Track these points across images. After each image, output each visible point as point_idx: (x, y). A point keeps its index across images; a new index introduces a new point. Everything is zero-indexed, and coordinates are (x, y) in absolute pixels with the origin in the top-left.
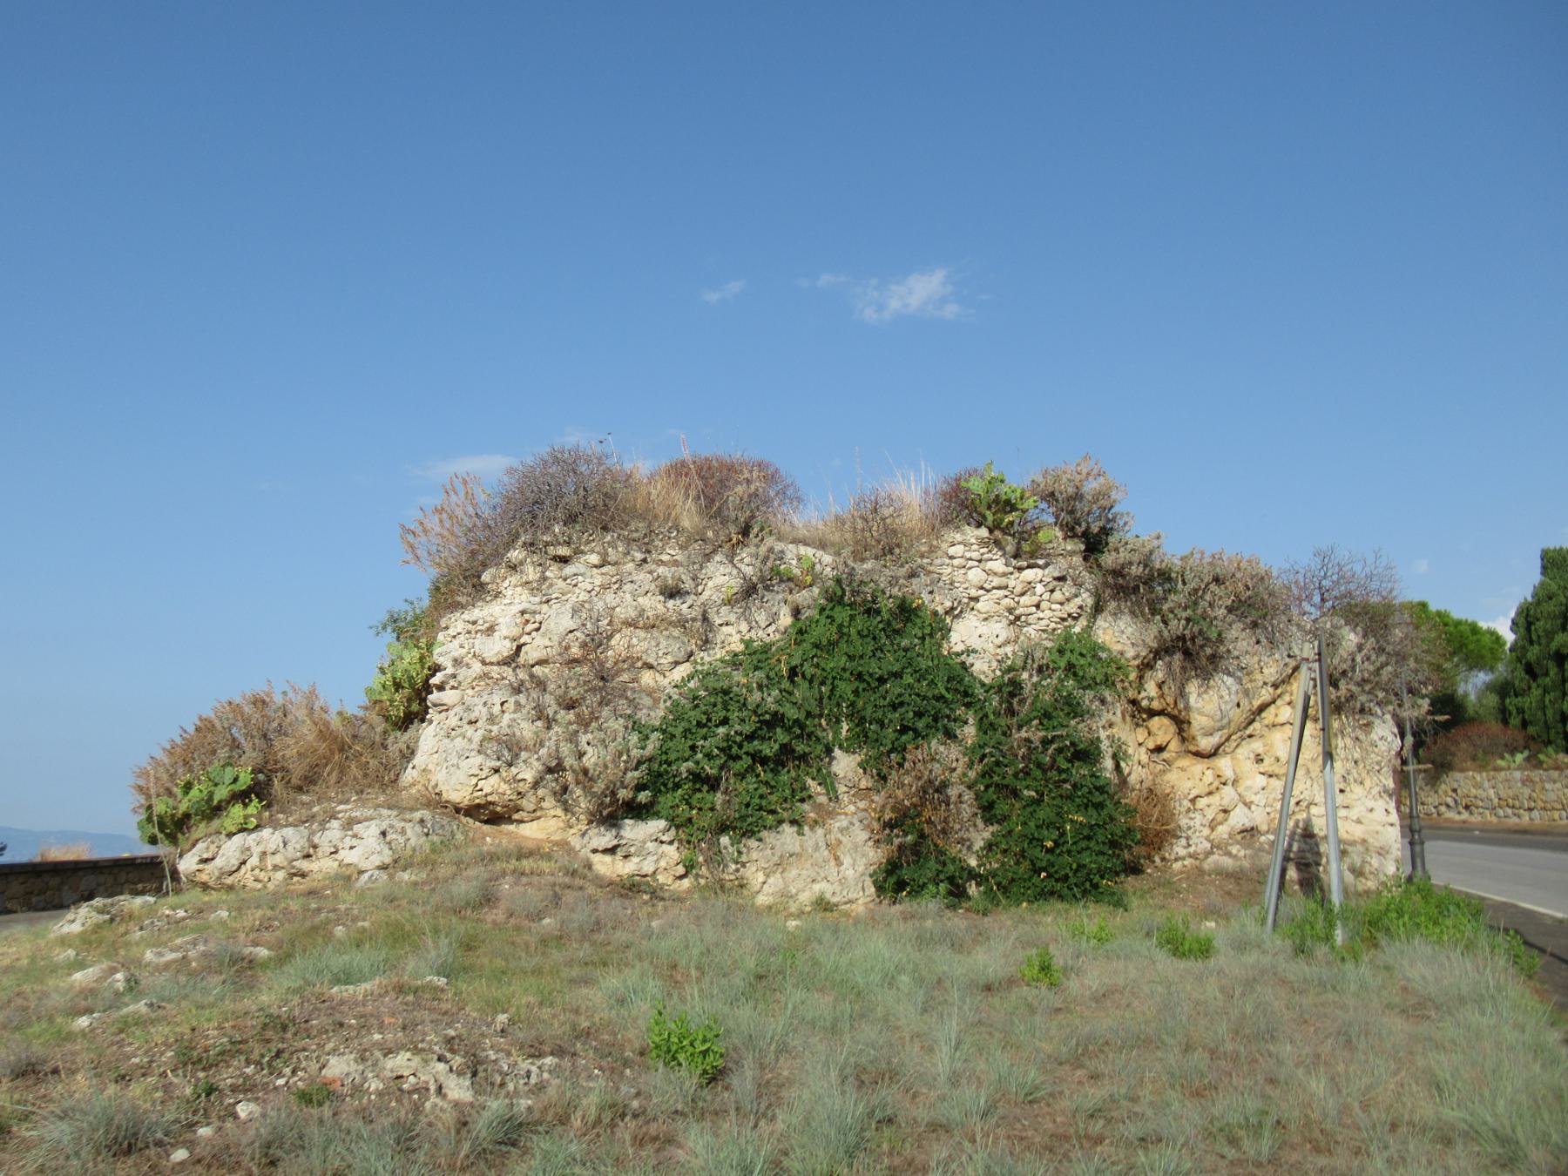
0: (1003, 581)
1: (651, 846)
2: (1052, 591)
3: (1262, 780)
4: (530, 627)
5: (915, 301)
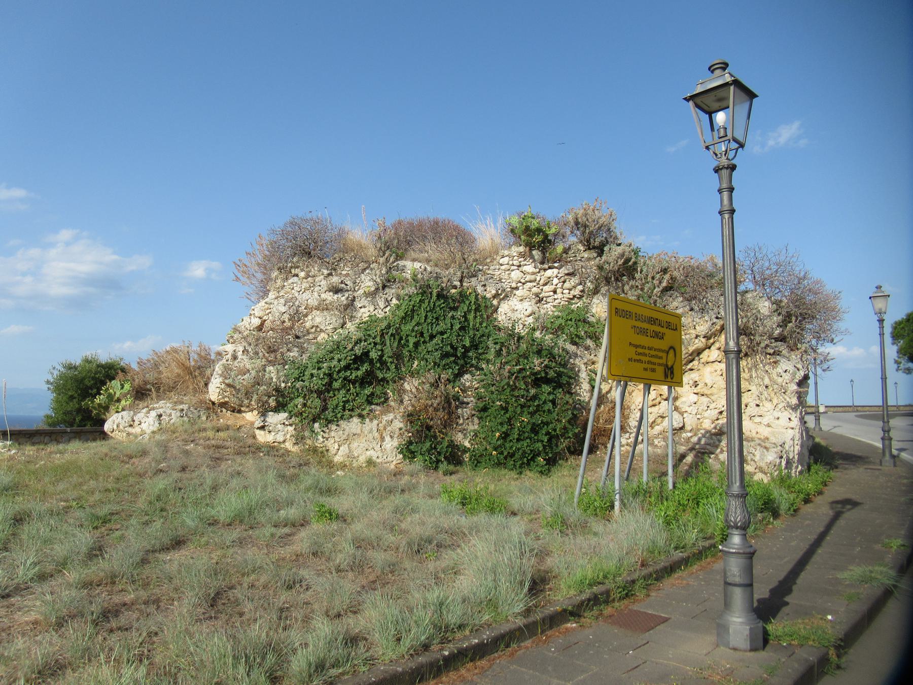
0: (533, 277)
1: (280, 427)
2: (564, 282)
3: (694, 398)
4: (268, 311)
5: (782, 140)
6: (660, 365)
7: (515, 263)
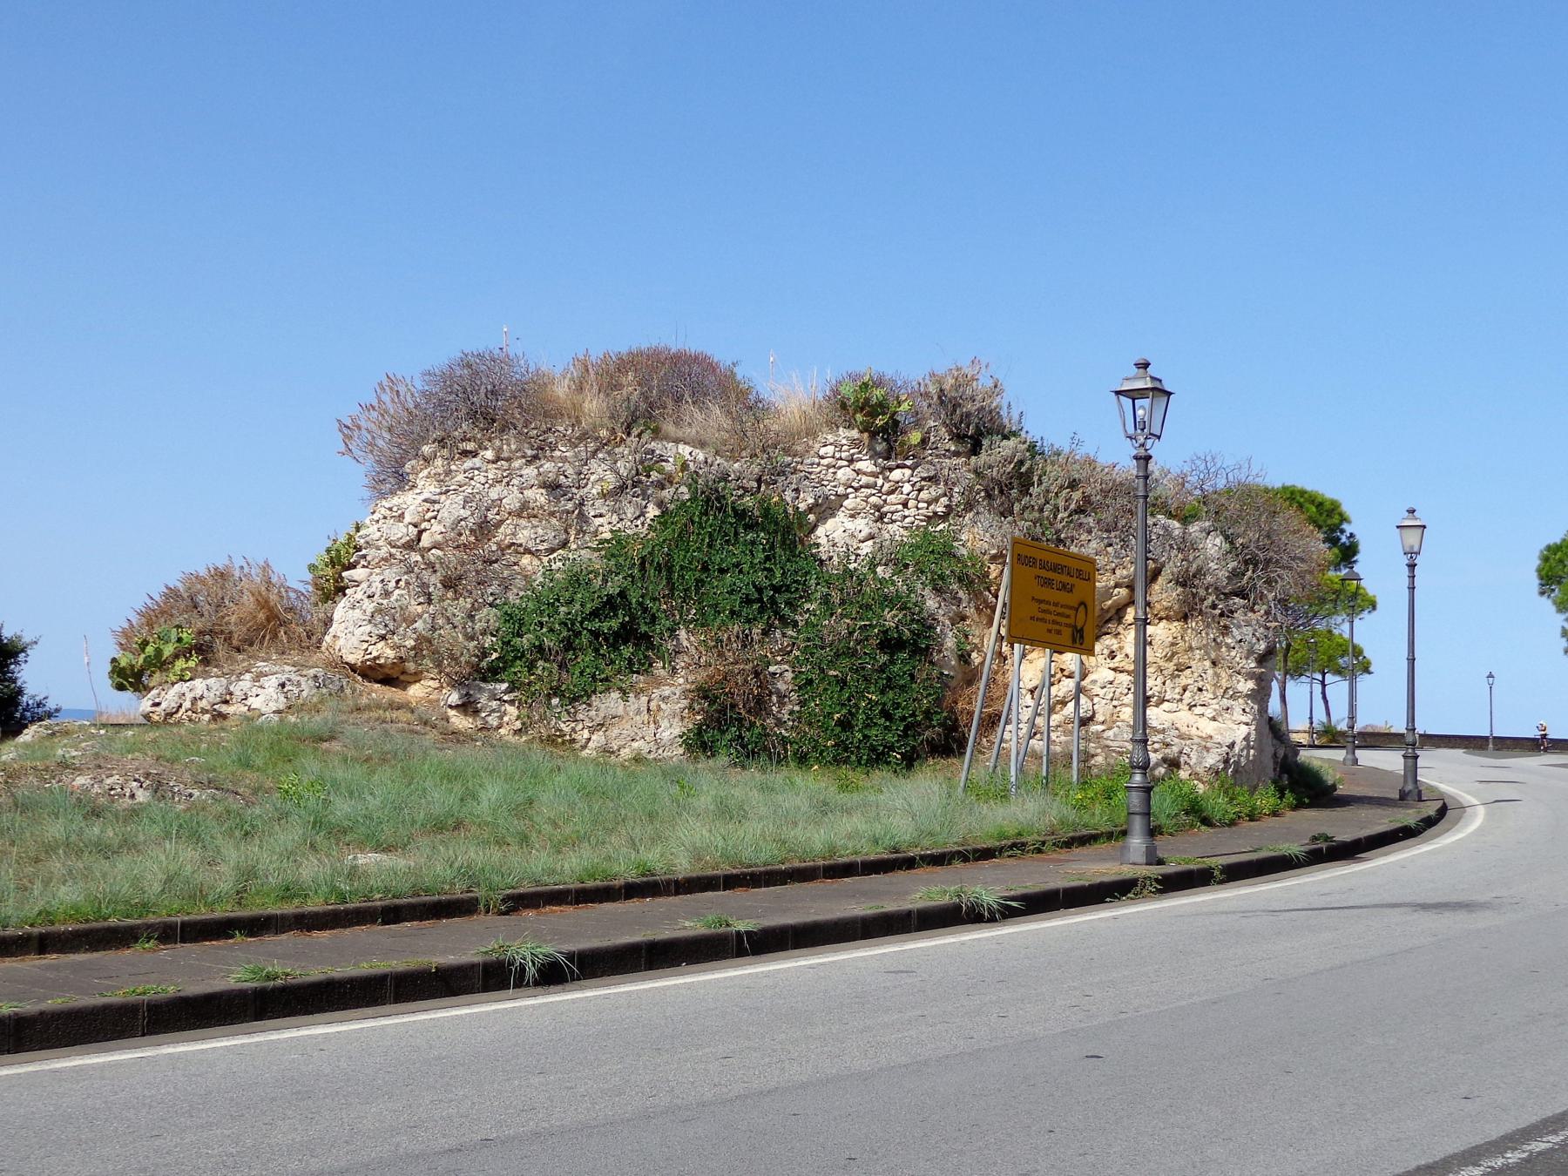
2: (920, 491)
3: (1111, 675)
4: (430, 514)
6: (1067, 625)
7: (844, 455)
